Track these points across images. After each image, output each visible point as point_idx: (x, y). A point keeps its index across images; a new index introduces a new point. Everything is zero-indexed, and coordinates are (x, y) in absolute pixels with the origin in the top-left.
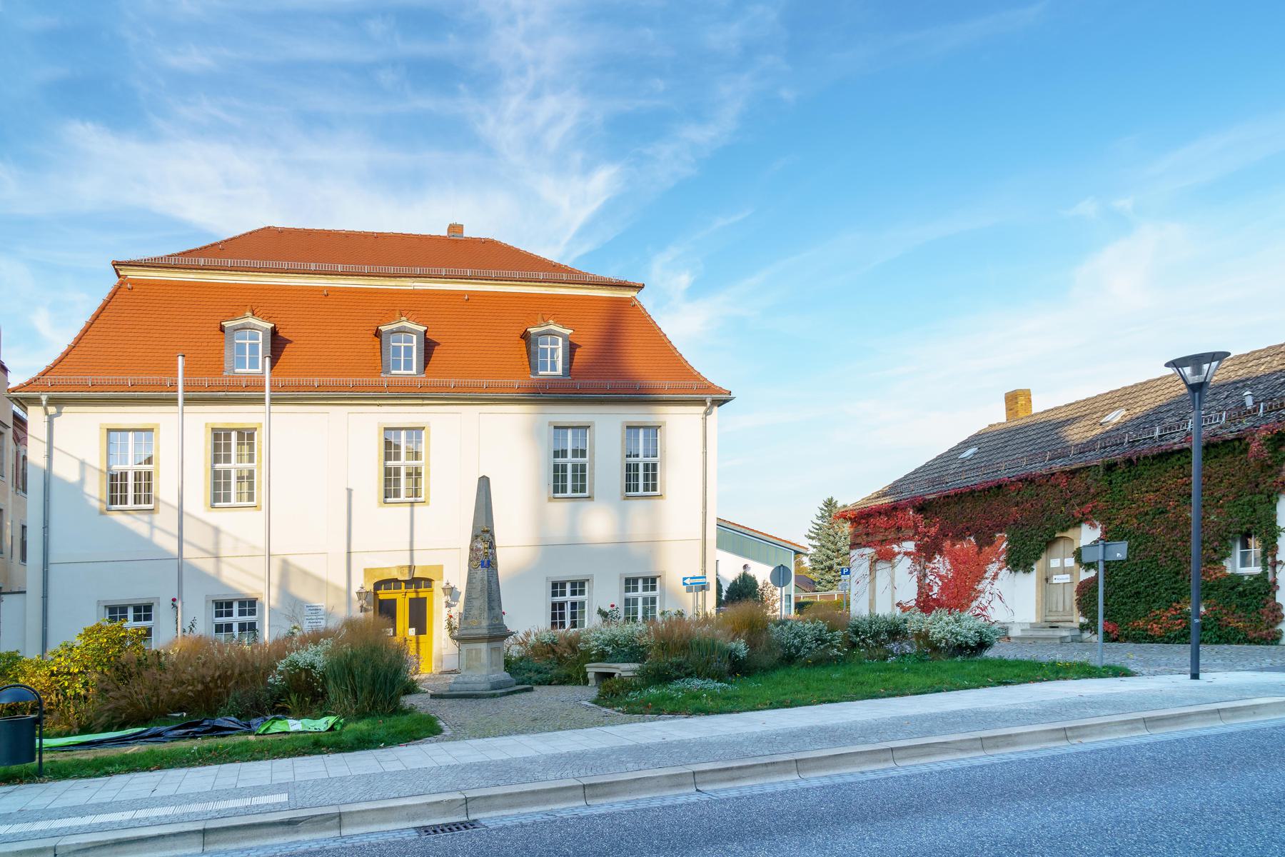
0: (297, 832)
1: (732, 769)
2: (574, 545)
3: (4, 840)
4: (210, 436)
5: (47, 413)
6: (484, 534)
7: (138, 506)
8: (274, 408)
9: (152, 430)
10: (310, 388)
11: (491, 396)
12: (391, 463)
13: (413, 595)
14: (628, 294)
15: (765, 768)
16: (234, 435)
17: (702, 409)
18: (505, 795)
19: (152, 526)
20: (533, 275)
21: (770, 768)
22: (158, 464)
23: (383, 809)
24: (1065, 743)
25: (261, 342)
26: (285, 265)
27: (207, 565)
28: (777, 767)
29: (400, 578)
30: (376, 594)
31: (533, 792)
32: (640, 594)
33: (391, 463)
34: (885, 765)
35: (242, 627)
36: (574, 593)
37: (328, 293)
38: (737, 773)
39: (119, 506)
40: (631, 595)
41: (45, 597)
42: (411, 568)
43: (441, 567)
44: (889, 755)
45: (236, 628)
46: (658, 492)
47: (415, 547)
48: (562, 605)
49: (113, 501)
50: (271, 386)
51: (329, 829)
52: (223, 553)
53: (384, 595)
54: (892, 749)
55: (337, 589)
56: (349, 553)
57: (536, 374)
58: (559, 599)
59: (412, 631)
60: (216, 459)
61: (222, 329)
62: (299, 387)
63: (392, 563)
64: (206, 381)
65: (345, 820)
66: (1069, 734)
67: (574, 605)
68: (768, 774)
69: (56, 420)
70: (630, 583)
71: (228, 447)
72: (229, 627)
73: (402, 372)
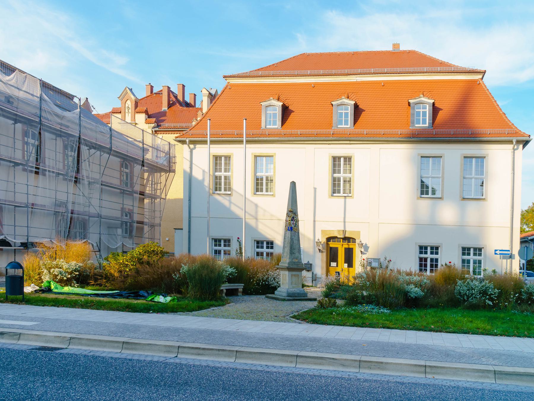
0: (3, 338)
1: (199, 348)
2: (433, 225)
3: (3, 326)
4: (331, 159)
5: (190, 148)
6: (293, 215)
7: (267, 193)
8: (248, 146)
9: (272, 156)
10: (296, 135)
11: (384, 139)
12: (336, 175)
13: (347, 246)
14: (478, 77)
15: (217, 352)
16: (342, 159)
17: (510, 146)
18: (87, 339)
19: (230, 202)
20: (434, 69)
21: (221, 352)
22: (232, 172)
23: (37, 335)
24: (423, 376)
25: (350, 111)
26: (334, 72)
27: (252, 222)
28: (224, 353)
29: (339, 237)
30: (327, 244)
31: (100, 341)
32: (472, 257)
33: (336, 175)
34: (289, 365)
35: (268, 254)
36: (225, 246)
37: (314, 86)
38: (201, 352)
39: (218, 192)
40: (466, 257)
41: (189, 232)
42: (344, 232)
43: (360, 232)
44: (294, 359)
45: (265, 254)
46: (483, 197)
47: (346, 221)
48: (426, 260)
49: (257, 190)
50: (246, 135)
51: (14, 339)
52: (259, 217)
53: (332, 244)
54: (297, 356)
55: (309, 239)
56: (314, 221)
57: (413, 126)
58: (466, 257)
59: (346, 265)
60: (334, 172)
61: (409, 104)
62: (291, 135)
63: (335, 228)
64: (220, 132)
65: (22, 337)
66: (428, 370)
67: (432, 260)
68: (219, 355)
69: (194, 151)
70: (465, 251)
71: (339, 165)
72: (262, 254)
73: (343, 126)
